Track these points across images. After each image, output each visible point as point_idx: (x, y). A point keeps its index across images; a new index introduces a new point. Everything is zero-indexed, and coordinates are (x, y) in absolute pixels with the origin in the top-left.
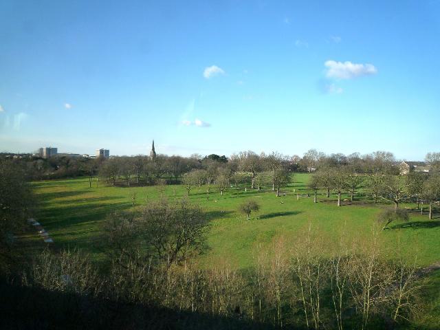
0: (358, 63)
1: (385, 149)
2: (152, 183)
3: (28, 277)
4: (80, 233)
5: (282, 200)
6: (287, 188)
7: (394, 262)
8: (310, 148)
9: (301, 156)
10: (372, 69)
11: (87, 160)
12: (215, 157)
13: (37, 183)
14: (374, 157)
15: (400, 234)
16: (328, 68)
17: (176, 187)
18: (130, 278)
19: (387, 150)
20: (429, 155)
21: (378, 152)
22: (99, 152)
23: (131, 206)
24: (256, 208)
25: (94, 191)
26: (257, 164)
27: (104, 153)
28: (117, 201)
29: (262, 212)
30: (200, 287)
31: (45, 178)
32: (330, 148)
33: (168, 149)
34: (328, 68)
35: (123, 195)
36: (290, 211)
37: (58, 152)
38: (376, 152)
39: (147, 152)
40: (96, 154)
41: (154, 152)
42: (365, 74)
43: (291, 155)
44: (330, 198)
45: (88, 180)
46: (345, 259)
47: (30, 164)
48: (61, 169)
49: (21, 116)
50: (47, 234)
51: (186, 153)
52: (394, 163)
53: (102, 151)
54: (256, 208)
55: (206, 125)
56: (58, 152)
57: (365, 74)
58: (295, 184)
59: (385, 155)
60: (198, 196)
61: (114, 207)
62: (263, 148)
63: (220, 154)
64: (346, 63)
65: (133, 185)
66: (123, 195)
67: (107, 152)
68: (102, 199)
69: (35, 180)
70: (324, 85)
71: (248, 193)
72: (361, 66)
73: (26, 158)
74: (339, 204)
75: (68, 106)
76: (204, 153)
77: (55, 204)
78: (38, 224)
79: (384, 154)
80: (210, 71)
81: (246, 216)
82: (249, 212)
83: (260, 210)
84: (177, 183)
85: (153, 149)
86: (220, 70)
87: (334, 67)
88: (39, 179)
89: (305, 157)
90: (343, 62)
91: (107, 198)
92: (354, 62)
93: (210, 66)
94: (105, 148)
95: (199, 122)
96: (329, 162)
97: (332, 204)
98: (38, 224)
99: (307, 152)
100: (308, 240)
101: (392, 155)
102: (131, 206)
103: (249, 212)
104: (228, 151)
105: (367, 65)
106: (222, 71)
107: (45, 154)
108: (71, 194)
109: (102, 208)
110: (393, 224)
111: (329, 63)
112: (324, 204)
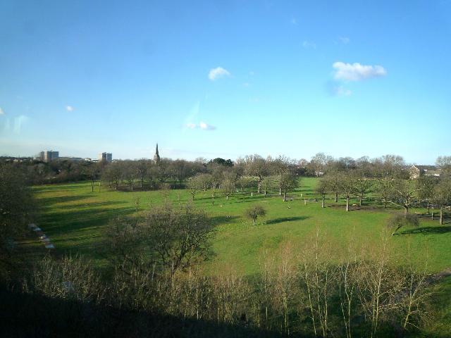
0: (367, 65)
1: (395, 152)
2: (156, 188)
3: (28, 283)
4: (82, 239)
5: (289, 204)
6: (295, 193)
7: (404, 268)
8: (317, 152)
9: (309, 160)
10: (381, 70)
11: (89, 164)
12: (220, 161)
13: (37, 187)
14: (384, 161)
15: (410, 239)
16: (336, 70)
17: (180, 191)
18: (134, 285)
19: (396, 154)
20: (440, 158)
21: (387, 156)
22: (101, 156)
23: (135, 211)
24: (263, 213)
25: (96, 196)
26: (264, 168)
27: (107, 157)
28: (119, 206)
29: (269, 217)
30: (205, 294)
31: (46, 183)
32: (338, 151)
33: (172, 152)
34: (336, 70)
35: (126, 200)
36: (297, 216)
37: (60, 156)
38: (385, 155)
39: (151, 156)
40: (98, 157)
41: (158, 156)
42: (374, 76)
43: (298, 159)
44: (338, 203)
45: (90, 184)
46: (353, 265)
47: (31, 168)
48: (63, 174)
49: (21, 119)
50: (48, 240)
51: (190, 156)
52: (404, 167)
53: (104, 155)
54: (263, 213)
55: (211, 128)
56: (60, 156)
57: (374, 76)
58: (302, 189)
59: (395, 159)
60: (203, 201)
61: (117, 212)
62: (269, 152)
63: (226, 158)
64: (354, 64)
65: (136, 189)
66: (126, 200)
67: (110, 155)
68: (105, 204)
69: (36, 185)
70: (332, 87)
71: (254, 198)
72: (370, 67)
73: (27, 162)
74: (347, 209)
75: (69, 108)
76: (209, 156)
77: (56, 209)
78: (39, 229)
79: (393, 157)
80: (216, 73)
81: (252, 222)
82: (255, 217)
83: (266, 215)
84: (182, 187)
85: (157, 153)
86: (225, 71)
87: (343, 69)
88: (40, 184)
89: (312, 161)
90: (352, 64)
91: (109, 203)
92: (363, 64)
93: (215, 68)
94: (108, 152)
95: (203, 125)
96: (337, 166)
97: (341, 209)
98: (39, 229)
99: (315, 155)
100: (316, 245)
101: (401, 159)
102: (135, 211)
103: (255, 217)
104: (234, 154)
105: (376, 66)
106: (228, 73)
107: (46, 158)
108: (73, 198)
109: (105, 213)
110: (403, 229)
111: (338, 65)
112: (332, 209)
